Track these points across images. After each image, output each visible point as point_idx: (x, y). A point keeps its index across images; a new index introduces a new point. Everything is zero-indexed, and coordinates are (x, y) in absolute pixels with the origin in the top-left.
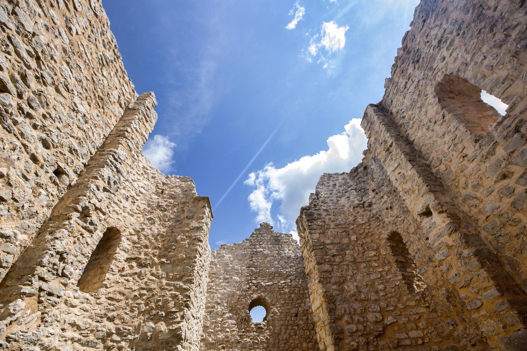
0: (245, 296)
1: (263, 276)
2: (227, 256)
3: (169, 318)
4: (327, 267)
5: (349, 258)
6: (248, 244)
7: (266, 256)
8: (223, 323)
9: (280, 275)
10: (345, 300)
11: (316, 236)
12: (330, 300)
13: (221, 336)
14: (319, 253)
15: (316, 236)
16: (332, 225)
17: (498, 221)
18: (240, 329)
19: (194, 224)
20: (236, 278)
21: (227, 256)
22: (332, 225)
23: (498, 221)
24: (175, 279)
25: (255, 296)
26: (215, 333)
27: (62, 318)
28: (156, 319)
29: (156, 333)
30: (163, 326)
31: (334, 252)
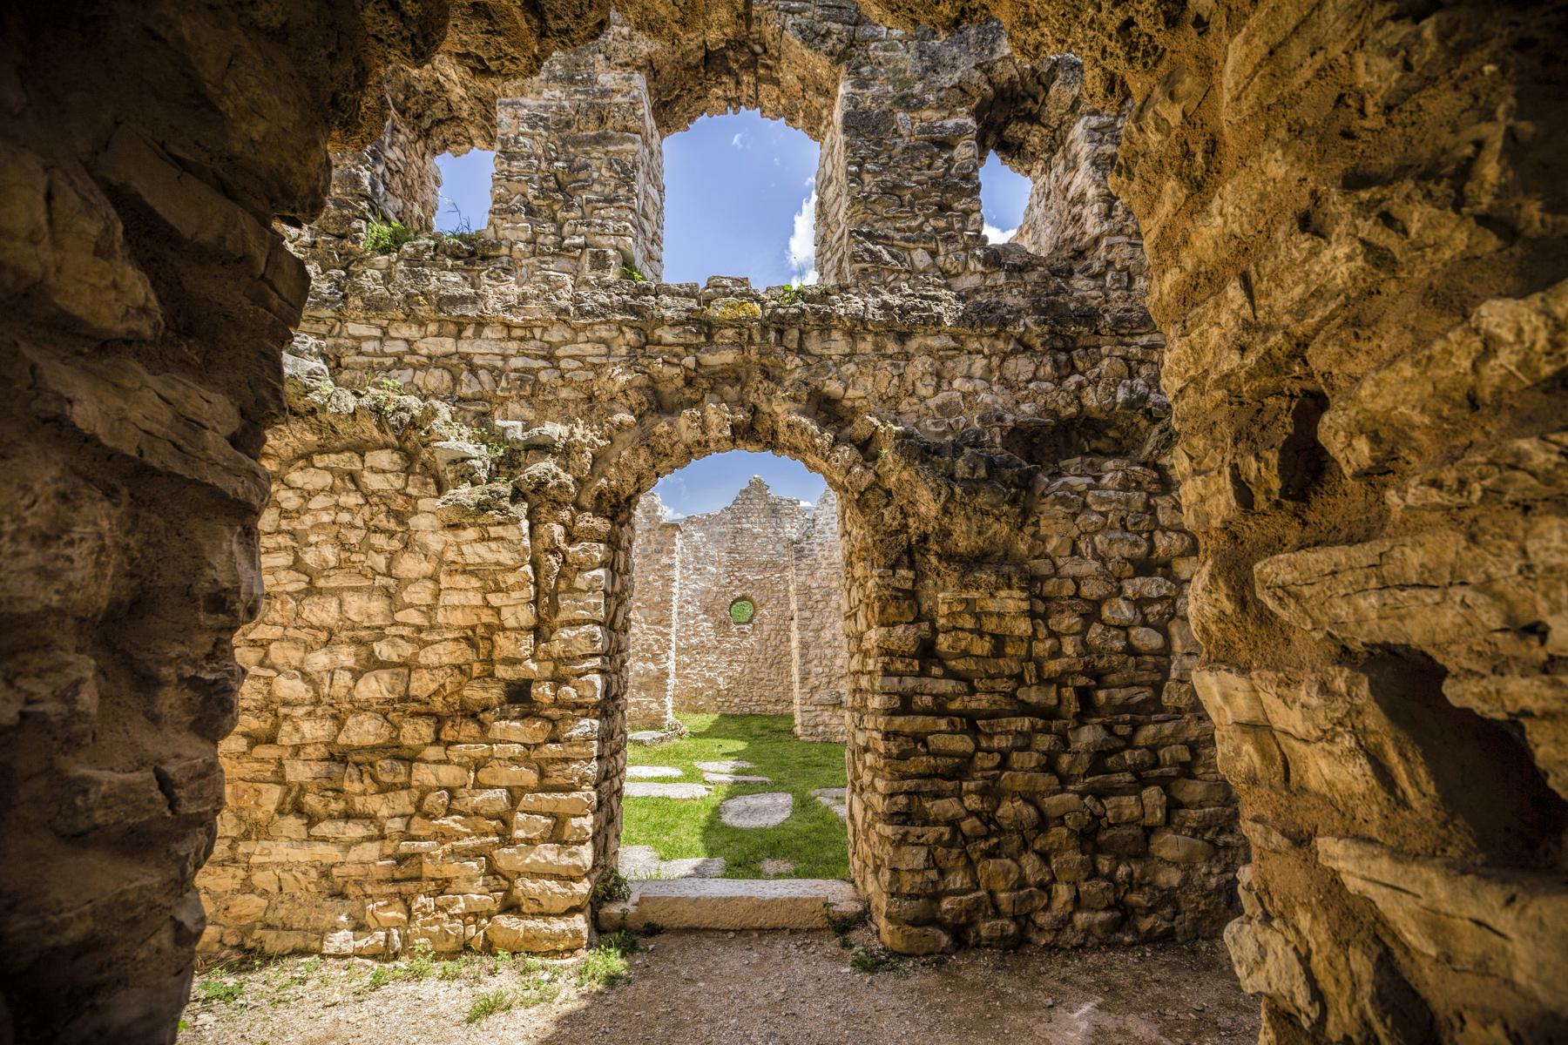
0: (725, 594)
1: (750, 567)
2: (697, 536)
3: (655, 658)
4: (807, 614)
5: (833, 604)
6: (729, 517)
7: (756, 537)
8: (696, 626)
9: (775, 565)
10: (818, 646)
11: (802, 578)
12: (804, 645)
13: (694, 641)
14: (803, 598)
15: (802, 578)
16: (824, 564)
17: (1148, 448)
18: (717, 633)
19: (665, 560)
20: (712, 569)
21: (697, 536)
22: (824, 564)
23: (1148, 448)
24: (653, 623)
25: (738, 594)
26: (687, 638)
27: (148, 395)
28: (645, 660)
29: (647, 672)
30: (651, 666)
31: (819, 597)
